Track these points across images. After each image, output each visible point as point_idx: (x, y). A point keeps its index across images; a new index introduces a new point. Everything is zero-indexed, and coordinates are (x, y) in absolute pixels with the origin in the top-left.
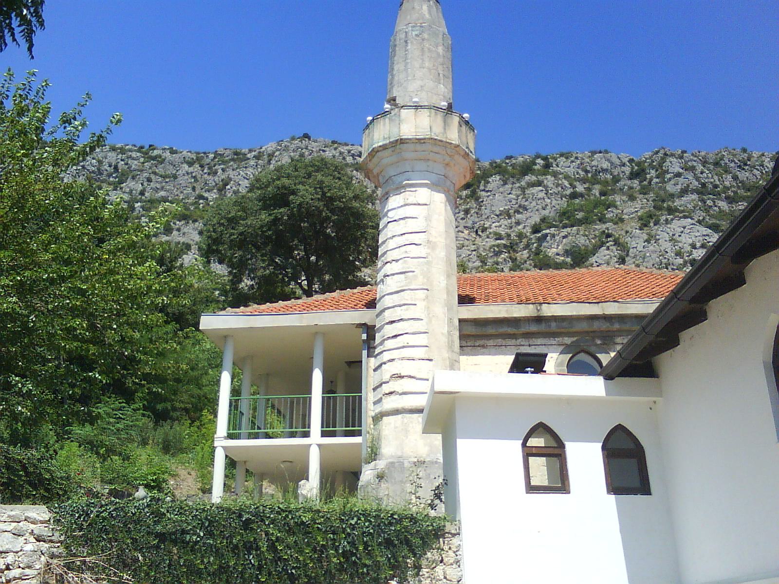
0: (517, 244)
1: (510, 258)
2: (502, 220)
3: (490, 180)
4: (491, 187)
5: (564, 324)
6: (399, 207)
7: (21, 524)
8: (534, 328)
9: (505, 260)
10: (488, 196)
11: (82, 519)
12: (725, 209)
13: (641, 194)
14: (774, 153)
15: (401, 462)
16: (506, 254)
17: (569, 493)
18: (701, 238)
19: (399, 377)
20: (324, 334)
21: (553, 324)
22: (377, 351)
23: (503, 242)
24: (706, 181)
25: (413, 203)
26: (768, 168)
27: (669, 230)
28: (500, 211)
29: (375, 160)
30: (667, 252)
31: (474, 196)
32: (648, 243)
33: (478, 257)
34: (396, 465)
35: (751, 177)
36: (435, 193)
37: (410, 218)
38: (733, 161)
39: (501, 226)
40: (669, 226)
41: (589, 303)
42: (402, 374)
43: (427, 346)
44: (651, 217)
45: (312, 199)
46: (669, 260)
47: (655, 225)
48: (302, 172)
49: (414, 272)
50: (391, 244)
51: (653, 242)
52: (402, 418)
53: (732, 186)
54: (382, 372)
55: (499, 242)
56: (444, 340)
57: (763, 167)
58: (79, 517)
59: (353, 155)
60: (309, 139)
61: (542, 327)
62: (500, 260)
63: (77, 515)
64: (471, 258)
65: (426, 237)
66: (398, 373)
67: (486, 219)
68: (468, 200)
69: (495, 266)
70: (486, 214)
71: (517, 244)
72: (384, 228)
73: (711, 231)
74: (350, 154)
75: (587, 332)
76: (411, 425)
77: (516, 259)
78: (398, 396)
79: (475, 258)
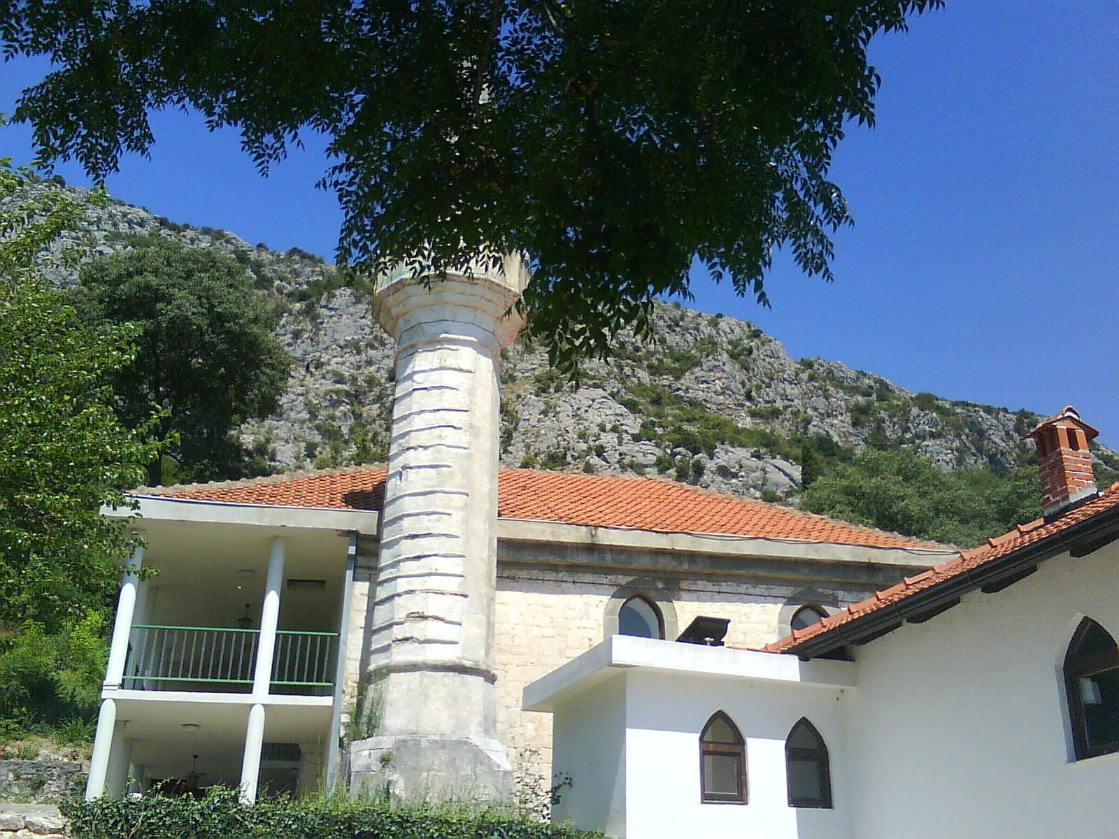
0: (365, 393)
1: (353, 413)
2: (348, 355)
3: (337, 293)
4: (337, 304)
5: (622, 557)
6: (431, 370)
7: (19, 833)
8: (582, 559)
9: (345, 414)
10: (331, 317)
11: (119, 828)
12: (645, 381)
13: (542, 345)
14: (714, 315)
15: (416, 740)
16: (348, 407)
17: (747, 804)
18: (613, 418)
19: (421, 617)
20: (286, 539)
21: (608, 556)
22: (382, 577)
23: (345, 387)
24: (626, 340)
25: (453, 367)
26: (704, 334)
27: (574, 401)
28: (346, 340)
29: (401, 295)
30: (567, 432)
31: (309, 312)
32: (545, 416)
33: (306, 405)
34: (409, 745)
35: (682, 343)
36: (481, 356)
37: (447, 387)
38: (662, 318)
39: (344, 364)
40: (573, 395)
41: (657, 532)
42: (426, 614)
43: (462, 576)
44: (551, 379)
45: (193, 314)
46: (569, 443)
47: (556, 392)
48: (179, 269)
49: (449, 467)
50: (418, 422)
51: (551, 415)
52: (421, 677)
53: (656, 352)
54: (393, 607)
55: (339, 386)
56: (483, 568)
57: (698, 332)
58: (115, 824)
59: (130, 222)
60: (63, 186)
61: (593, 560)
62: (338, 414)
63: (111, 822)
64: (296, 406)
65: (468, 419)
66: (420, 611)
67: (324, 349)
68: (301, 318)
69: (330, 421)
70: (324, 342)
71: (365, 393)
72: (404, 397)
73: (626, 410)
74: (125, 219)
75: (647, 571)
76: (432, 688)
77: (361, 414)
78: (416, 644)
79: (301, 407)
